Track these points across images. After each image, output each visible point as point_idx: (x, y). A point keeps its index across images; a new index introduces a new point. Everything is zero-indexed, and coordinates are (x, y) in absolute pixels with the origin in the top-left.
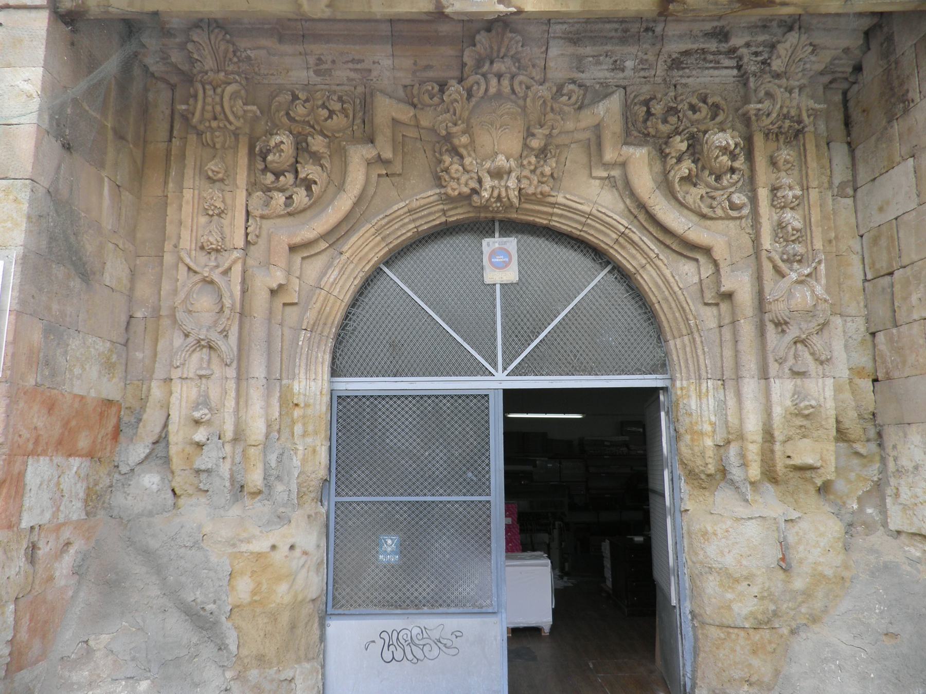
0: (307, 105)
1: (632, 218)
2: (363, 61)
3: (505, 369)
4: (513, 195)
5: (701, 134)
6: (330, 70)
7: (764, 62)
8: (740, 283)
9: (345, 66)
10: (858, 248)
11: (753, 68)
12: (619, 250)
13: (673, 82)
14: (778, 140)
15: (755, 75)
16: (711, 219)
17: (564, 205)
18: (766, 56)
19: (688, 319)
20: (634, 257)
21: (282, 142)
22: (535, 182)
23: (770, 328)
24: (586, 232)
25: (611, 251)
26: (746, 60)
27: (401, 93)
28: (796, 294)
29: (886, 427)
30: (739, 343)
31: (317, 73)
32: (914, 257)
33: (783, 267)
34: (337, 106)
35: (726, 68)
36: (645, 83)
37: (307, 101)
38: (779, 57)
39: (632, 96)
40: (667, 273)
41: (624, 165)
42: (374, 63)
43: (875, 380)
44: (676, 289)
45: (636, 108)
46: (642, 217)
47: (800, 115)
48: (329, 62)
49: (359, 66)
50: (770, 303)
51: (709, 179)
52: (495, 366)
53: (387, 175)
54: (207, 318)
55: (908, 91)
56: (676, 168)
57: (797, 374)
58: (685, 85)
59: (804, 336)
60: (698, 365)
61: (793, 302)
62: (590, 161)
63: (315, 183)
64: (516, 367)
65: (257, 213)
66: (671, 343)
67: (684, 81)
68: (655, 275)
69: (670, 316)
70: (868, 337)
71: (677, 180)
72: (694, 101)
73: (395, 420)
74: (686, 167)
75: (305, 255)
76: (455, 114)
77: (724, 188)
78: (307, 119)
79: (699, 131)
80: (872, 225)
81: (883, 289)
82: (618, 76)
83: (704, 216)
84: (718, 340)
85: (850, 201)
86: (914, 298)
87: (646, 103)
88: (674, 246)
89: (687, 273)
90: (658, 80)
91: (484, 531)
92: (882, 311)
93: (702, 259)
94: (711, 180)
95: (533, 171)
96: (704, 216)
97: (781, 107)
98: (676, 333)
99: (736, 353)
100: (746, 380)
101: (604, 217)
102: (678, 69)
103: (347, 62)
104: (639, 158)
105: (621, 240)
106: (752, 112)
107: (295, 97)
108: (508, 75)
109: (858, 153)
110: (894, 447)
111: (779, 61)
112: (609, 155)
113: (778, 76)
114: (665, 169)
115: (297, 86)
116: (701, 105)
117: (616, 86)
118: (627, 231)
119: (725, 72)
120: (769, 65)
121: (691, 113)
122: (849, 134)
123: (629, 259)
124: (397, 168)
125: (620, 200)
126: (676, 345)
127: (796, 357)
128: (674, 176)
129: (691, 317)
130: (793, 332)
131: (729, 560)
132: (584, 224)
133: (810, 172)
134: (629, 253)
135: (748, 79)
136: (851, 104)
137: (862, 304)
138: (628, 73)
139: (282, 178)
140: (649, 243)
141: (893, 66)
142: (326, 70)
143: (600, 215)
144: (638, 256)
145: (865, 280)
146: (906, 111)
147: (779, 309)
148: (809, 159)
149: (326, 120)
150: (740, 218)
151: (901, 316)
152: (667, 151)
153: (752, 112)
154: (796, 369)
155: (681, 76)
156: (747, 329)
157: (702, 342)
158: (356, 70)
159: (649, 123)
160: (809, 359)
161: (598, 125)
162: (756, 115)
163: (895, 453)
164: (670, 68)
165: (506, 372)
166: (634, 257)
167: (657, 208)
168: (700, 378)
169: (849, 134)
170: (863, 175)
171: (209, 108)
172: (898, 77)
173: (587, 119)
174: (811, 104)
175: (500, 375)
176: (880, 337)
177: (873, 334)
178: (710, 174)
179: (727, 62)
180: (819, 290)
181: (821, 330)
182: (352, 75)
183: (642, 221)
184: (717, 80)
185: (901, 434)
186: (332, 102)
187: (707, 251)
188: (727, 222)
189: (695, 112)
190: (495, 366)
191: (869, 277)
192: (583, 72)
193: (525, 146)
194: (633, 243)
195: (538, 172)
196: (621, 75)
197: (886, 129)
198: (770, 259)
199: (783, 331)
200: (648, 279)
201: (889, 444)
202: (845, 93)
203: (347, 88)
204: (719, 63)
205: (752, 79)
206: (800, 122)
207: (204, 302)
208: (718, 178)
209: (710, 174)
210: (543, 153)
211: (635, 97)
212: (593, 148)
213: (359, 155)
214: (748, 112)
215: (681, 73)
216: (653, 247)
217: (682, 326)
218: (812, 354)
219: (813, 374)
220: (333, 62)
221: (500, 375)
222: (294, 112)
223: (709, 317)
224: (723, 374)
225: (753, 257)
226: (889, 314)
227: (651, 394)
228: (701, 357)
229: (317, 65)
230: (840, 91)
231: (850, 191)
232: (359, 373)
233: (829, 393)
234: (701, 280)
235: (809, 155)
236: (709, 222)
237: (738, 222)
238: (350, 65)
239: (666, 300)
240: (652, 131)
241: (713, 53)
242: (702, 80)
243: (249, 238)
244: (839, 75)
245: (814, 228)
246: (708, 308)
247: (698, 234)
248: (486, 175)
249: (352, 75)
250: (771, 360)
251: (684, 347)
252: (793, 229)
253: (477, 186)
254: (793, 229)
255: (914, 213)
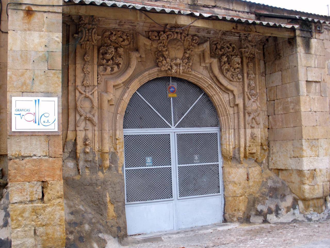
0: (116, 36)
1: (212, 79)
2: (134, 23)
3: (174, 126)
4: (181, 71)
5: (230, 56)
6: (123, 25)
7: (246, 37)
8: (240, 101)
9: (128, 24)
10: (265, 91)
11: (244, 38)
12: (208, 89)
13: (223, 38)
14: (249, 59)
15: (243, 40)
16: (232, 81)
17: (194, 75)
18: (247, 35)
19: (226, 111)
20: (212, 92)
21: (113, 51)
22: (187, 68)
23: (247, 114)
24: (199, 83)
25: (205, 89)
26: (242, 35)
27: (144, 33)
28: (253, 105)
29: (270, 142)
30: (240, 119)
31: (119, 25)
32: (280, 98)
33: (250, 97)
34: (125, 37)
35: (236, 36)
36: (215, 38)
37: (115, 35)
38: (250, 37)
39: (212, 41)
40: (222, 97)
41: (211, 64)
42: (137, 24)
43: (268, 129)
44: (224, 102)
45: (213, 45)
46: (215, 79)
47: (254, 53)
48: (123, 22)
49: (133, 24)
50: (247, 107)
51: (232, 70)
52: (172, 125)
53: (141, 61)
54: (88, 110)
55: (280, 53)
56: (224, 66)
57: (252, 127)
58: (225, 39)
59: (254, 117)
60: (229, 125)
61: (252, 107)
62: (200, 61)
63: (120, 64)
64: (178, 125)
65: (102, 73)
66: (221, 118)
67: (225, 38)
68: (218, 97)
69: (221, 110)
70: (267, 117)
71: (224, 69)
72: (229, 45)
73: (144, 142)
74: (227, 66)
75: (116, 88)
76: (163, 44)
77: (236, 72)
78: (116, 41)
79: (230, 55)
80: (270, 86)
81: (272, 104)
82: (208, 35)
83: (231, 80)
84: (233, 118)
85: (264, 78)
86: (279, 108)
87: (215, 44)
88: (223, 89)
89: (226, 97)
90: (219, 37)
91: (170, 176)
92: (271, 110)
93: (230, 93)
94: (233, 70)
95: (186, 64)
96: (231, 80)
97: (250, 51)
98: (223, 115)
99: (239, 122)
100: (241, 129)
101: (205, 79)
102: (224, 35)
103: (129, 23)
104: (215, 61)
105: (209, 86)
106: (243, 51)
107: (112, 33)
108: (180, 33)
109: (267, 64)
110: (272, 147)
111: (250, 38)
112: (207, 61)
113: (249, 41)
114: (220, 65)
115: (111, 29)
116: (230, 47)
117: (207, 37)
118: (211, 84)
119: (236, 37)
120: (248, 38)
121: (227, 49)
122: (264, 58)
123: (210, 92)
124: (144, 60)
125: (208, 73)
126: (222, 119)
127: (252, 123)
128: (224, 68)
129: (227, 111)
130: (252, 116)
131: (235, 180)
132: (199, 81)
133: (256, 70)
134: (211, 90)
135: (242, 40)
136: (265, 50)
137: (266, 107)
138: (211, 35)
139: (109, 62)
140: (217, 88)
141: (277, 45)
142: (122, 24)
143: (204, 79)
144: (213, 91)
145: (267, 101)
146: (280, 58)
147: (249, 109)
148: (256, 66)
149: (122, 42)
150: (240, 82)
151: (276, 112)
152: (222, 60)
153: (243, 51)
154: (252, 126)
155: (225, 37)
156: (241, 114)
157: (230, 118)
158: (131, 25)
159: (217, 51)
160: (255, 123)
161: (204, 50)
162: (244, 52)
163: (272, 148)
164: (222, 35)
165: (175, 127)
166: (212, 92)
167: (220, 78)
168: (229, 129)
169: (264, 58)
170: (268, 71)
171: (87, 37)
172: (278, 49)
173: (201, 48)
174: (257, 50)
175: (173, 127)
176: (270, 117)
177: (269, 116)
178: (233, 68)
179: (237, 35)
180: (258, 103)
181: (258, 115)
182: (130, 27)
183: (215, 81)
184: (234, 39)
185: (274, 143)
186: (124, 36)
187: (232, 92)
188: (236, 83)
189: (229, 49)
190: (172, 125)
191: (268, 100)
192: (199, 33)
193: (184, 55)
194: (212, 87)
195: (188, 64)
196: (209, 35)
197: (274, 61)
198: (247, 95)
199: (250, 115)
200: (216, 99)
201: (271, 146)
202: (263, 46)
203: (127, 30)
204: (235, 35)
205: (243, 41)
206: (254, 55)
207: (87, 104)
208: (235, 70)
209: (233, 68)
210: (188, 58)
211: (213, 42)
212: (202, 57)
213: (134, 56)
214: (242, 51)
215: (225, 36)
216: (218, 89)
217: (225, 113)
218: (256, 122)
219: (256, 127)
220: (125, 22)
221: (173, 127)
222: (112, 38)
223: (231, 111)
224: (234, 127)
225: (242, 93)
226: (273, 111)
227: (214, 136)
228: (230, 123)
229: (119, 23)
230: (262, 46)
231: (264, 75)
232: (130, 127)
233: (259, 133)
234: (229, 100)
235: (256, 65)
236: (232, 82)
237: (239, 83)
238: (130, 24)
239: (221, 105)
240: (217, 53)
241: (234, 32)
242: (230, 39)
243: (98, 82)
244: (263, 41)
245: (257, 86)
246: (231, 108)
247: (230, 87)
248: (174, 65)
249: (130, 27)
250: (247, 123)
251: (225, 119)
252: (253, 86)
253: (170, 68)
254: (253, 86)
255: (281, 86)
